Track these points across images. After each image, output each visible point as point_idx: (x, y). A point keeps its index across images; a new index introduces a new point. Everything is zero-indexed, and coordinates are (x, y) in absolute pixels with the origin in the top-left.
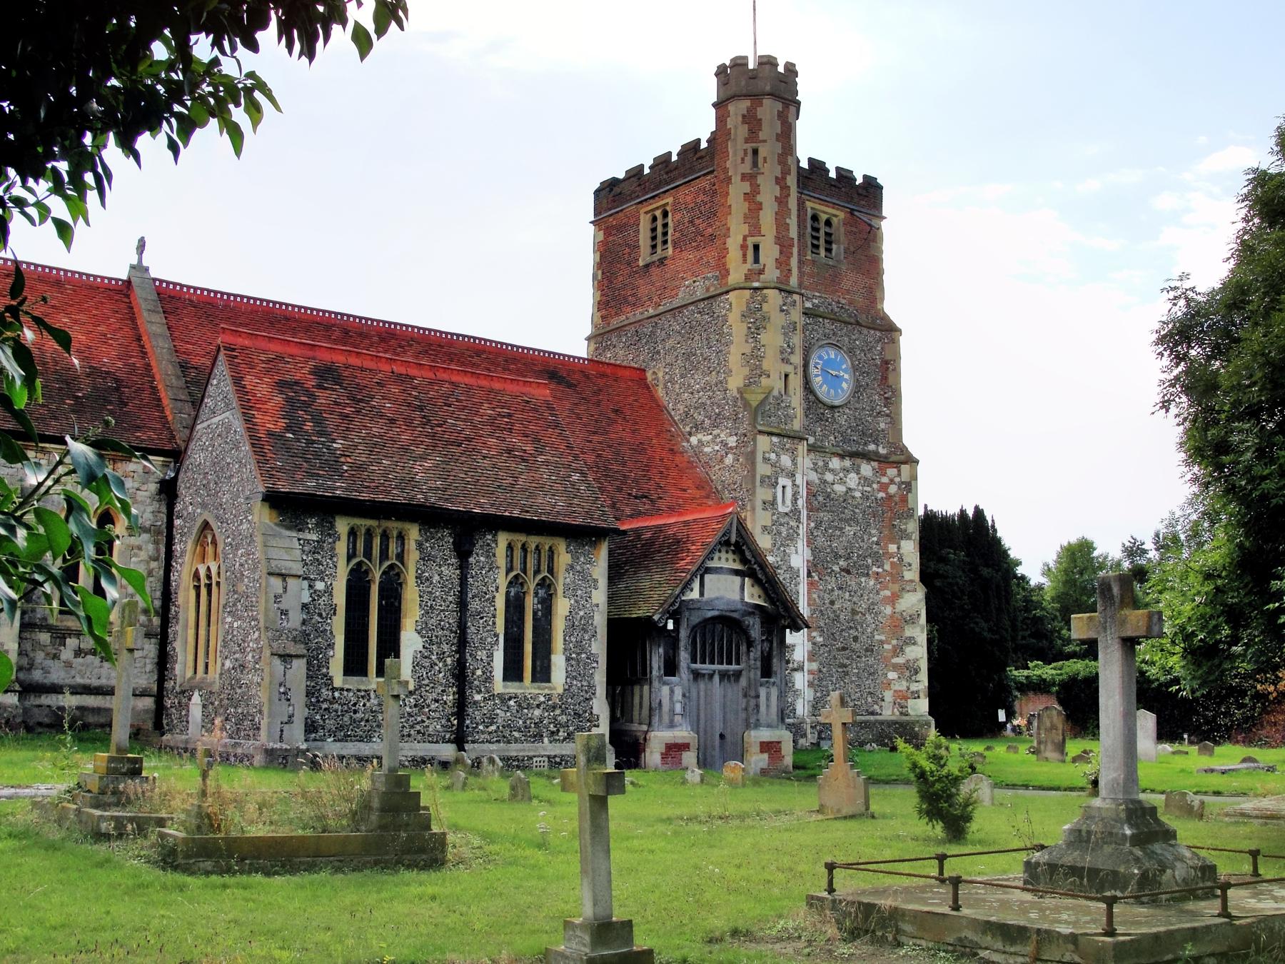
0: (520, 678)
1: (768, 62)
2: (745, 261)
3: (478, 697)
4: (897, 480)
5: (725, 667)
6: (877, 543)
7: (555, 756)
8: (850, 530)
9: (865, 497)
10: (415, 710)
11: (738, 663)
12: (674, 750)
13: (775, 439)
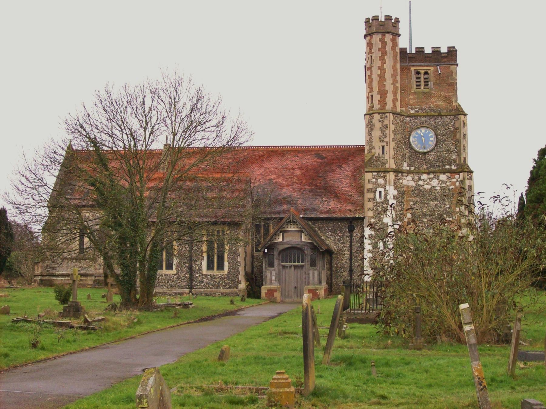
0: (213, 269)
1: (388, 18)
2: (368, 103)
3: (197, 275)
4: (459, 180)
5: (297, 264)
6: (449, 208)
7: (224, 293)
8: (433, 204)
9: (442, 189)
10: (177, 279)
11: (303, 262)
12: (271, 292)
13: (375, 174)
